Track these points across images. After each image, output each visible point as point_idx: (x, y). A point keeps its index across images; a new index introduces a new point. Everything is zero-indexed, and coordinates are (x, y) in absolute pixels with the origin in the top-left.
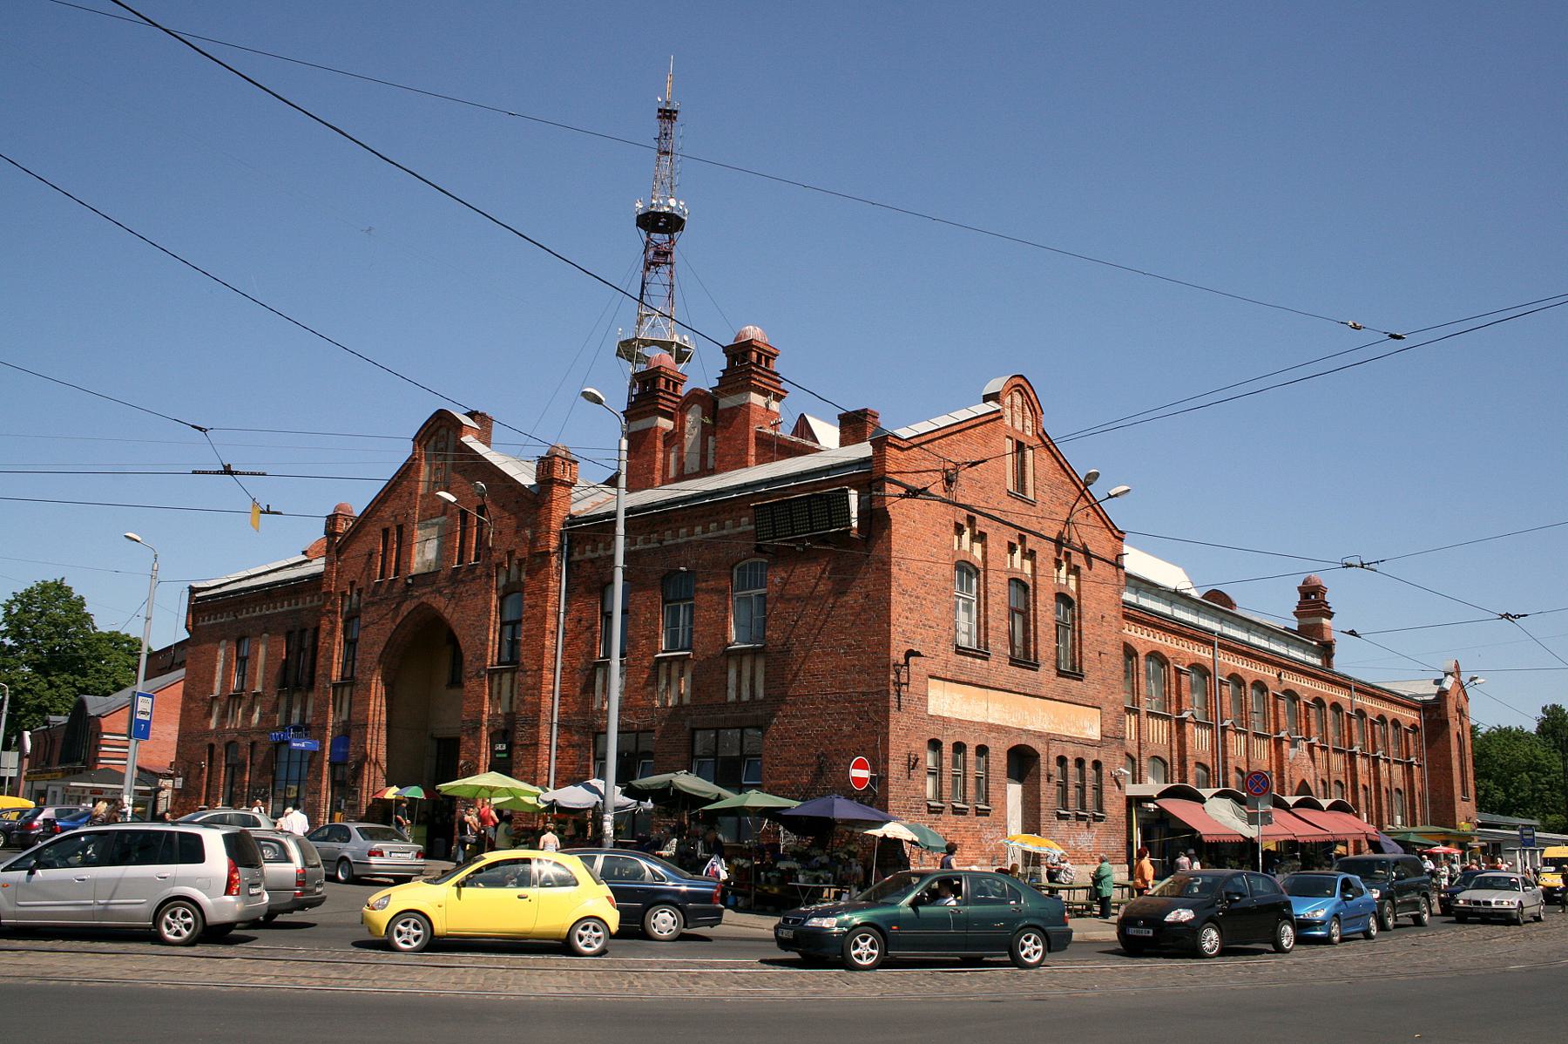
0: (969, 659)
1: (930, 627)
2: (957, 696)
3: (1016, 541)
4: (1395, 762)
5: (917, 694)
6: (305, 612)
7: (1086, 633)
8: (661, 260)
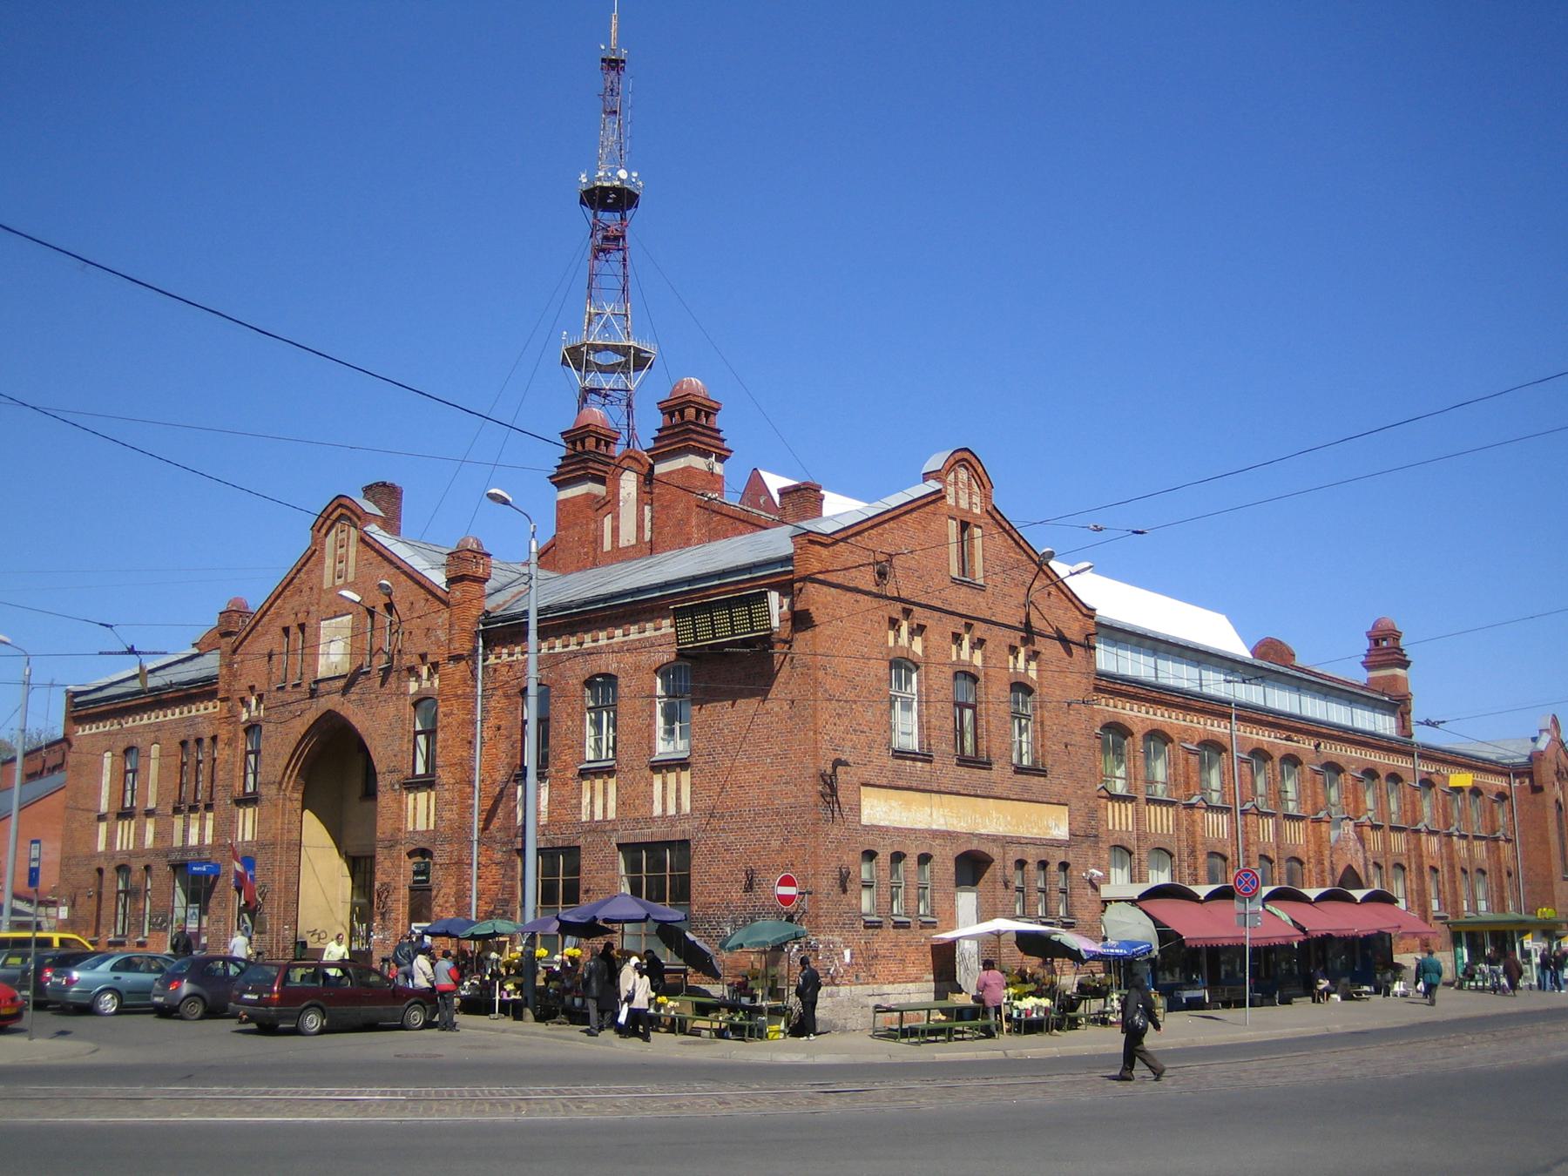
0: (908, 763)
1: (861, 732)
2: (894, 804)
3: (962, 631)
4: (1476, 838)
5: (848, 804)
6: (200, 719)
7: (1049, 723)
8: (611, 245)
